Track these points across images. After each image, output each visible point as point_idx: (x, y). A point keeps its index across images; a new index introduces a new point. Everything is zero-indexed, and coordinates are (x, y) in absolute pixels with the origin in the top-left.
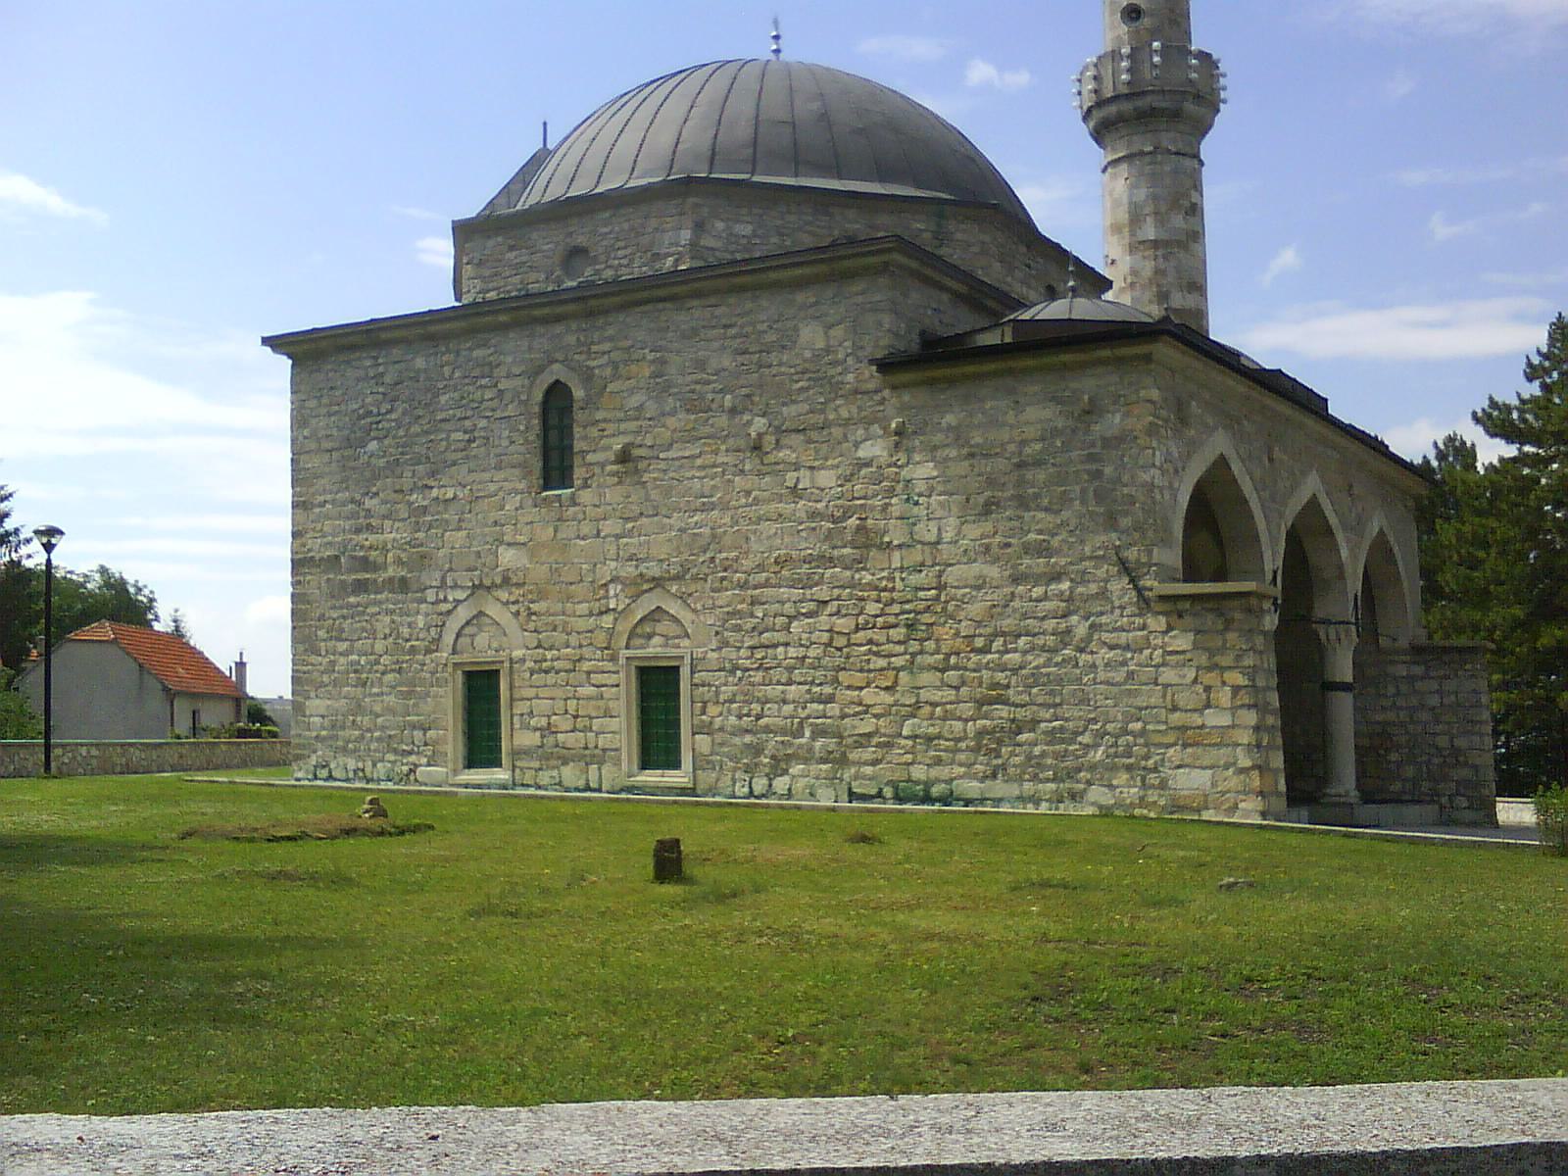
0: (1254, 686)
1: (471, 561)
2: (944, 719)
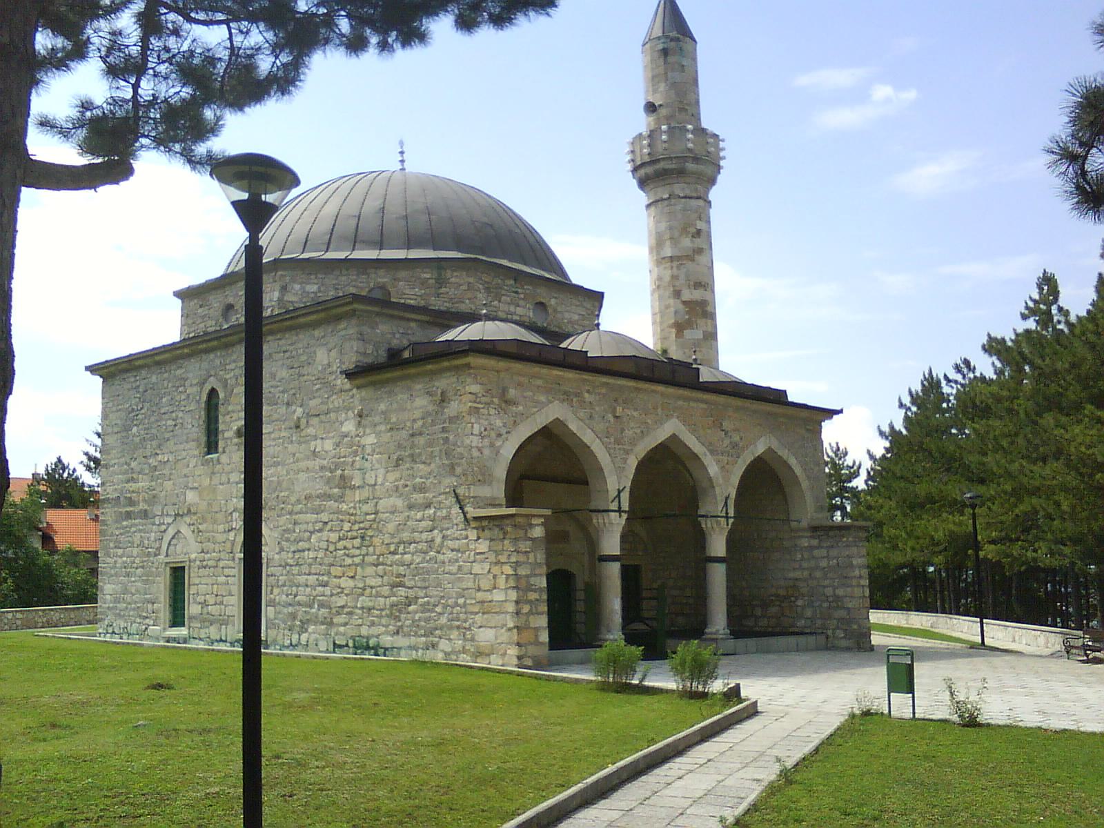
0: (516, 575)
1: (174, 500)
2: (377, 596)
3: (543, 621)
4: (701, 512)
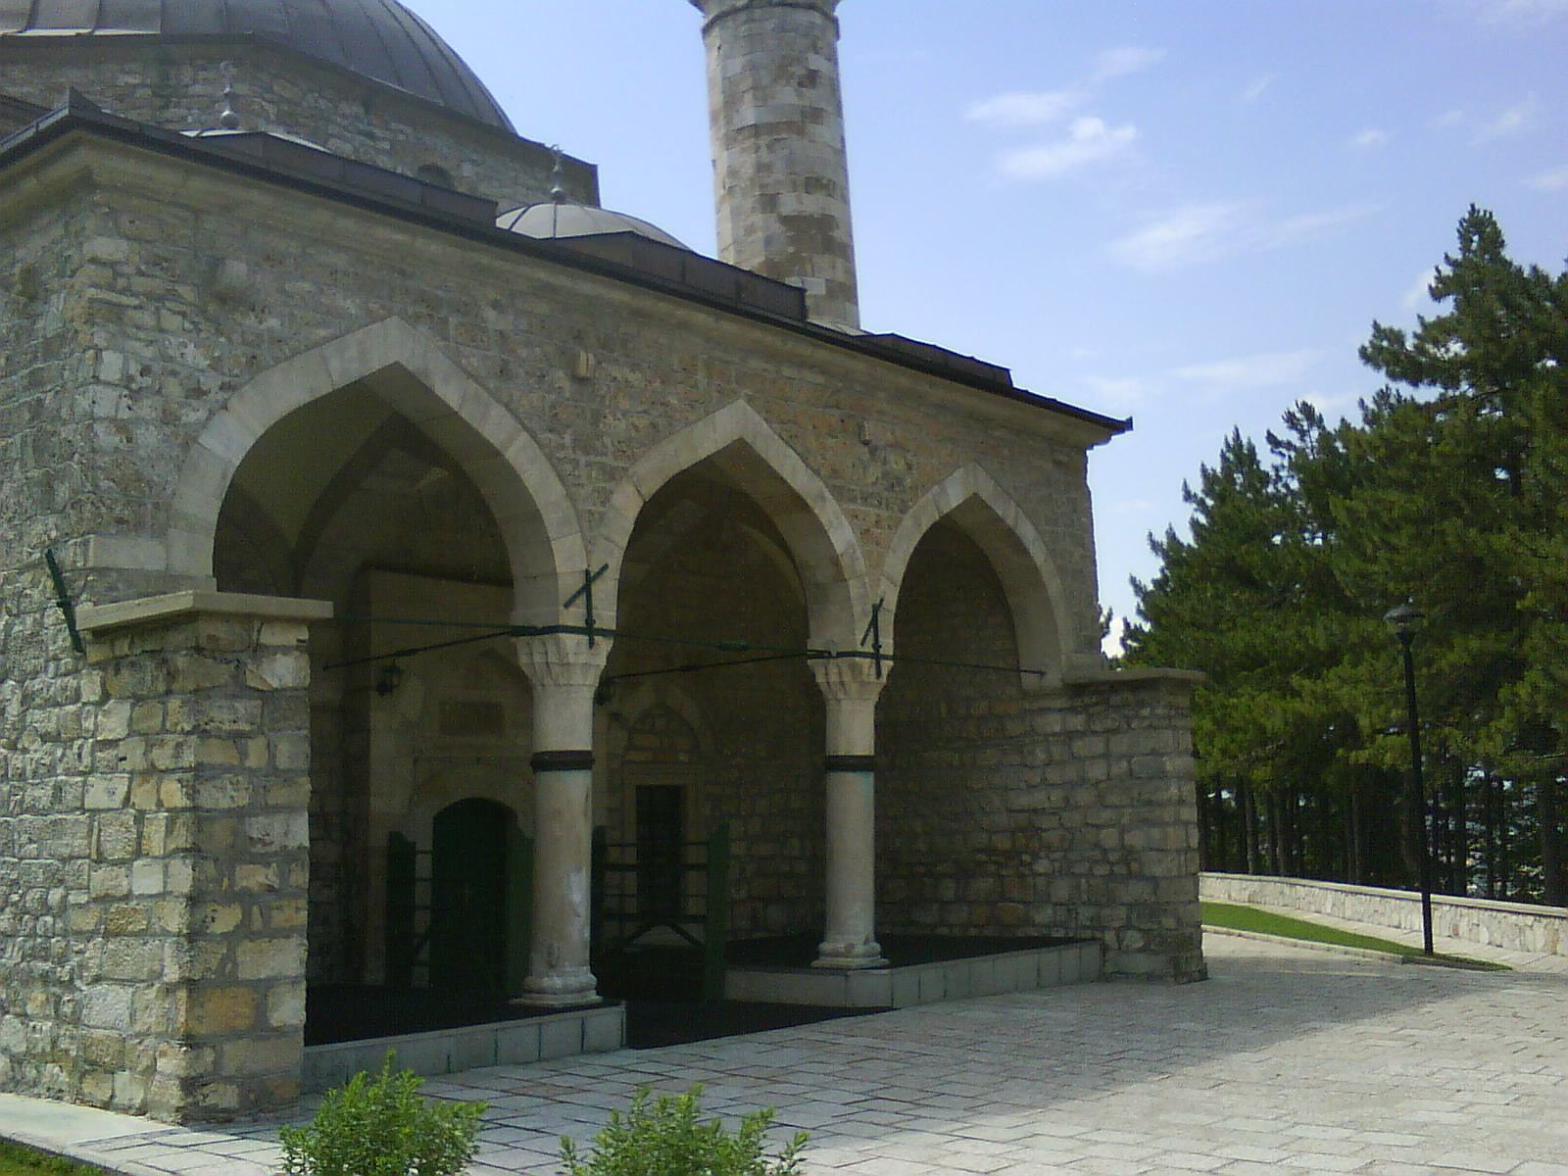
0: (195, 808)
3: (289, 959)
4: (815, 643)
